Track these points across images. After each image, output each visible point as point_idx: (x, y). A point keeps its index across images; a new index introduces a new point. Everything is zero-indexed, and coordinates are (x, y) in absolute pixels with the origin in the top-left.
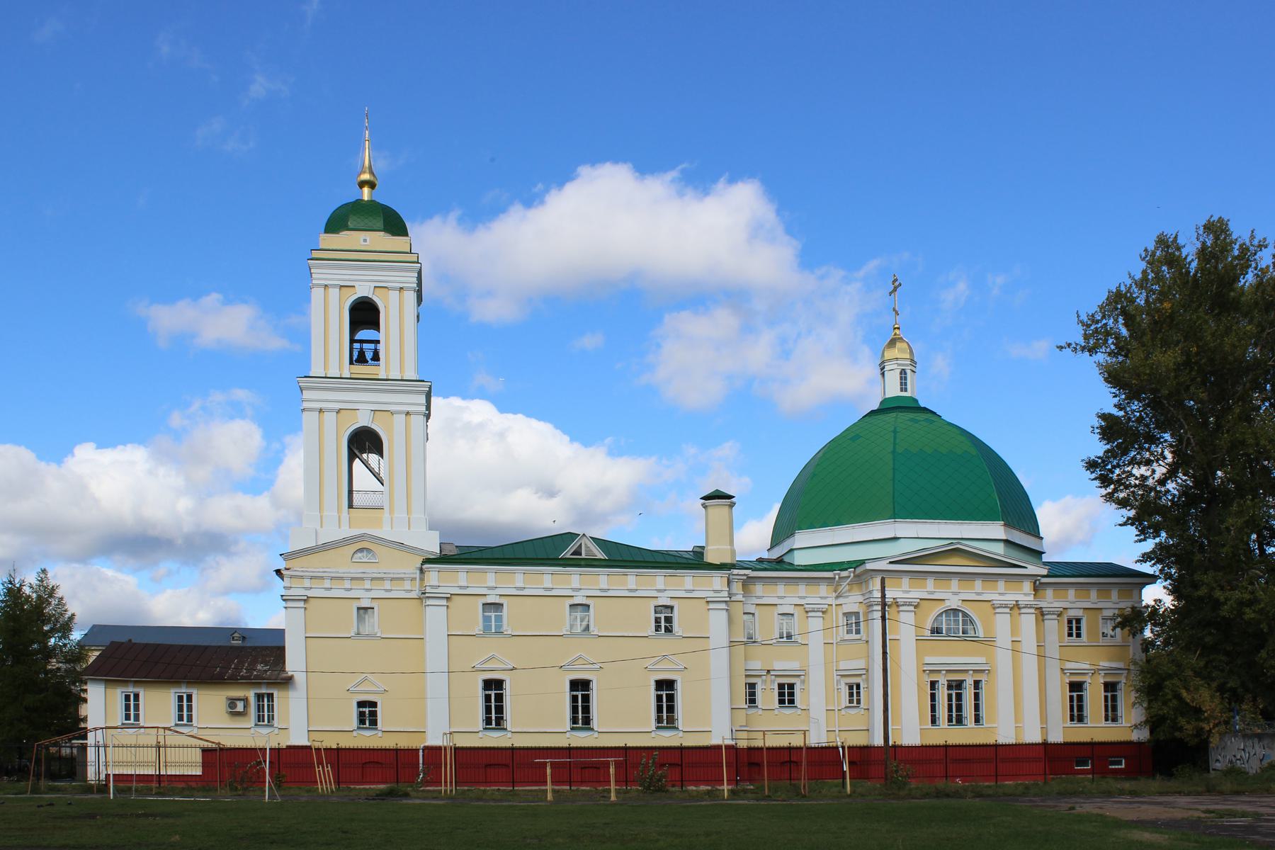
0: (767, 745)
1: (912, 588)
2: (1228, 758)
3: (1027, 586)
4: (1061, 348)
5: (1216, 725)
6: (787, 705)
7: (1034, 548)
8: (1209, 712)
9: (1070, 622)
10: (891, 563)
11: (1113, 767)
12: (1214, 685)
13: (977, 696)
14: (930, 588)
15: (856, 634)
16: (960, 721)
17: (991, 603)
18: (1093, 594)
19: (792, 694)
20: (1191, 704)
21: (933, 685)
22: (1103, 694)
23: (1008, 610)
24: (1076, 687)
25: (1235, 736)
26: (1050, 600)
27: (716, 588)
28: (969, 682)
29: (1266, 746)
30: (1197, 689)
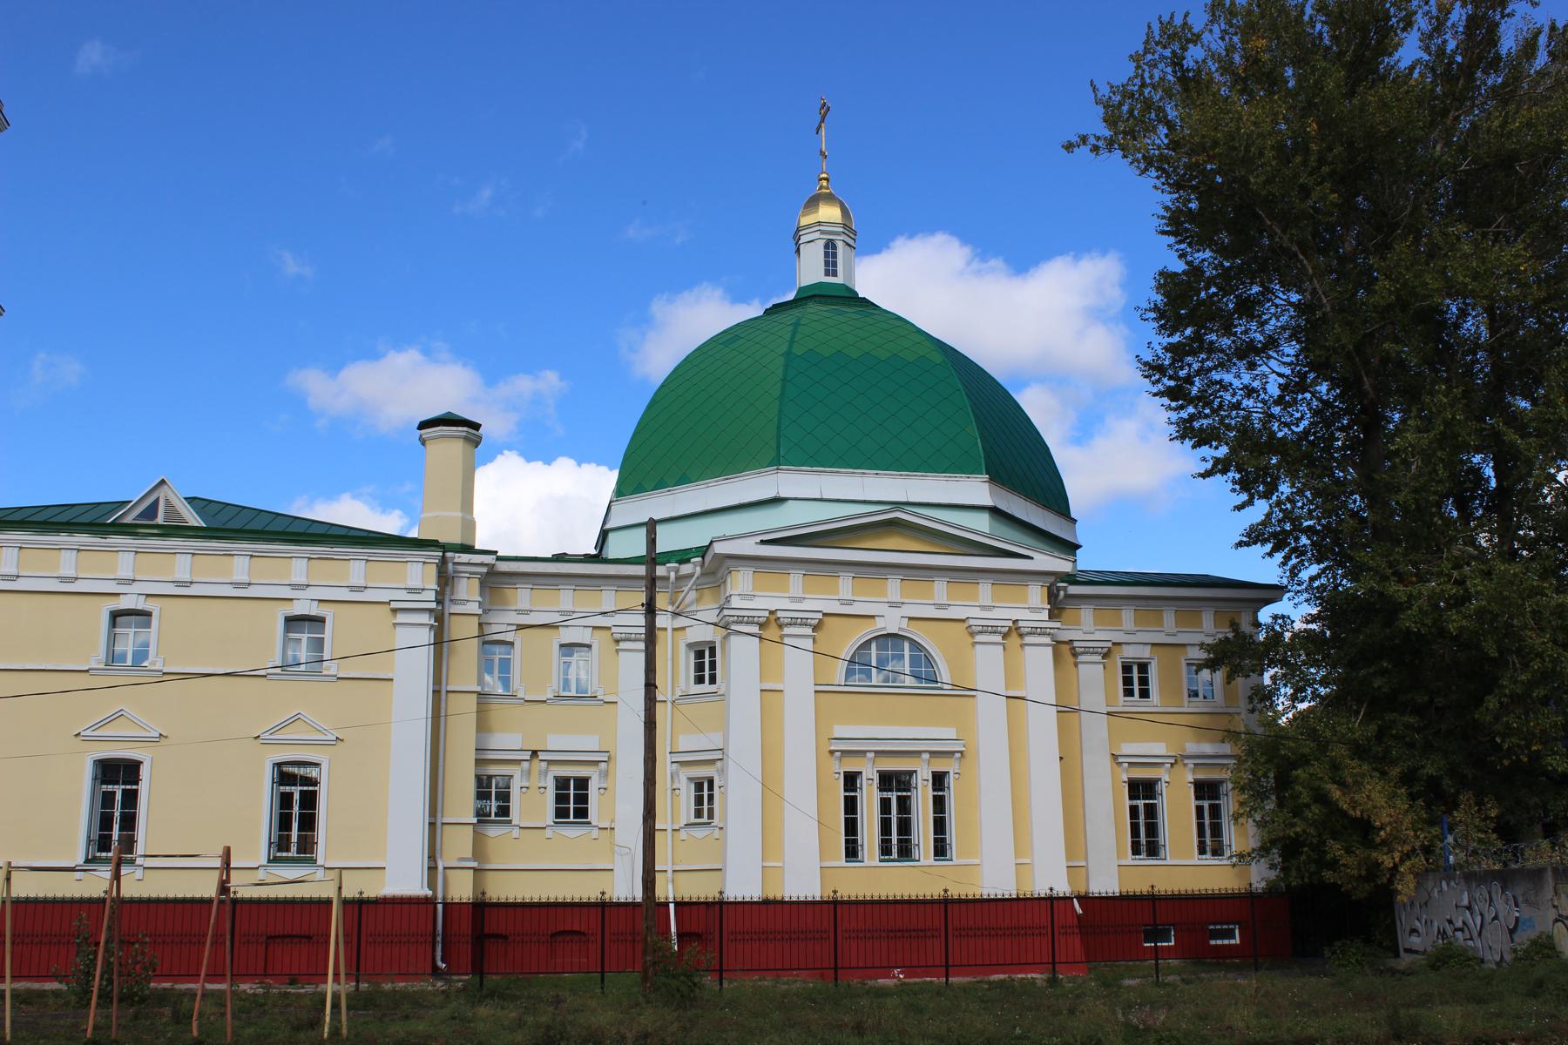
0: (14, 894)
1: (807, 593)
2: (1436, 924)
3: (1036, 594)
4: (1069, 147)
5: (1406, 856)
6: (572, 819)
7: (1044, 528)
8: (1388, 829)
9: (1127, 668)
10: (763, 542)
11: (1219, 942)
12: (1395, 772)
13: (939, 804)
14: (843, 593)
15: (710, 684)
16: (906, 852)
17: (966, 625)
18: (1169, 618)
19: (582, 799)
20: (1351, 812)
21: (851, 780)
22: (1193, 803)
23: (998, 638)
24: (1142, 789)
25: (1449, 879)
26: (1086, 627)
27: (411, 584)
28: (924, 774)
29: (1520, 899)
30: (1358, 784)
